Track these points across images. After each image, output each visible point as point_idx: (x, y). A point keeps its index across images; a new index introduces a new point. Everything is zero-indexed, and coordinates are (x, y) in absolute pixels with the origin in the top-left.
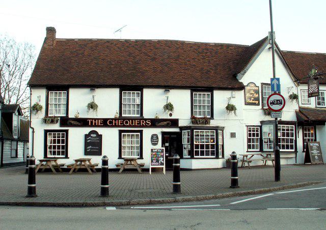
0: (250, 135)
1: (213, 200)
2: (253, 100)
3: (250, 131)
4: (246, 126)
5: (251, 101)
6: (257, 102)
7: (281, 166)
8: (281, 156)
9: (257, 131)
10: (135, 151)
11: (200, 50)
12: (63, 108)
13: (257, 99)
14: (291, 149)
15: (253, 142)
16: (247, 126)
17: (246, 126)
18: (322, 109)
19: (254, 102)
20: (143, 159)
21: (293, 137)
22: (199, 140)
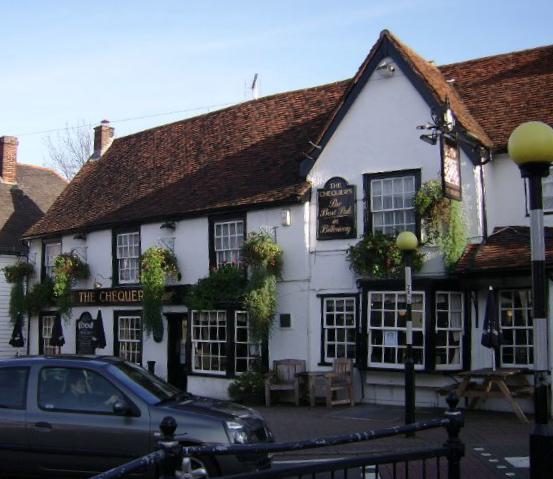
0: (330, 319)
1: (302, 452)
2: (337, 226)
3: (330, 309)
4: (318, 296)
5: (332, 229)
6: (348, 229)
7: (528, 452)
8: (418, 383)
9: (349, 309)
10: (346, 343)
11: (214, 284)
12: (410, 467)
13: (350, 221)
14: (386, 361)
15: (341, 338)
16: (322, 297)
17: (318, 296)
18: (184, 331)
19: (339, 230)
20: (419, 170)
21: (373, 331)
22: (397, 300)
